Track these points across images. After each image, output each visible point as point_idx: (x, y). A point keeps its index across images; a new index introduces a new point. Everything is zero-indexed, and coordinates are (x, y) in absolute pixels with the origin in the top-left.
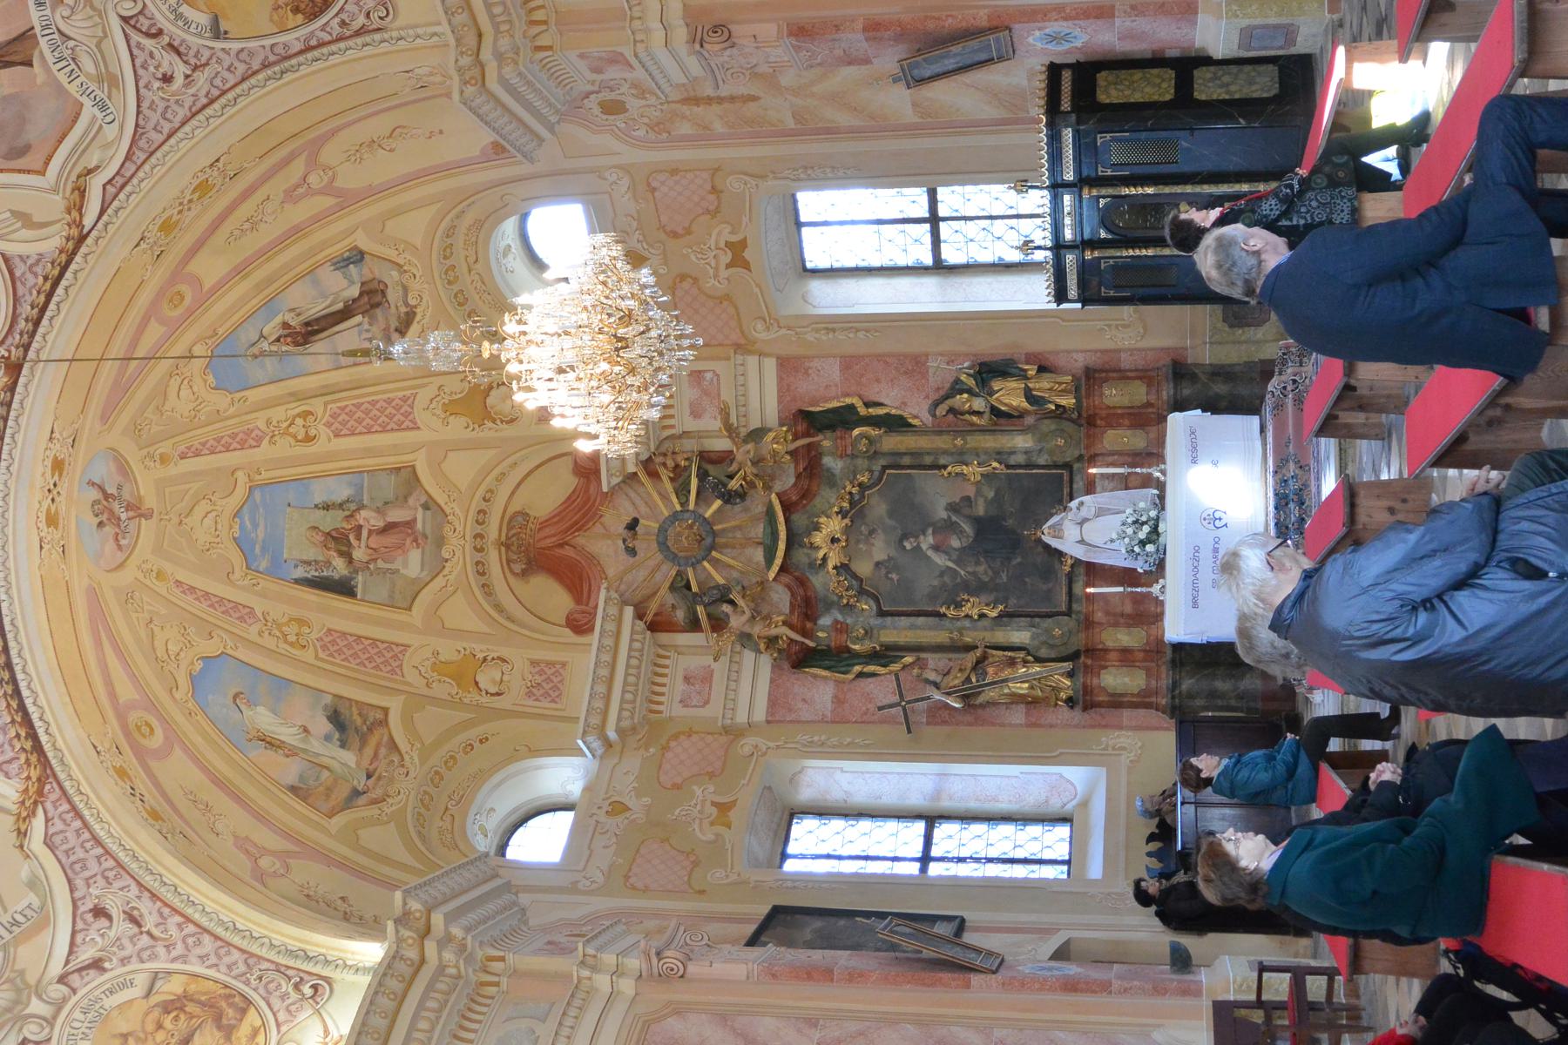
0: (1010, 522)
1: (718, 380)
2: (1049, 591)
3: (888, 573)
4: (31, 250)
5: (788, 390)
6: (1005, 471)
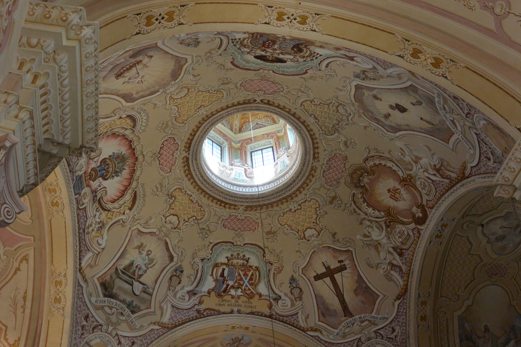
4: (300, 319)
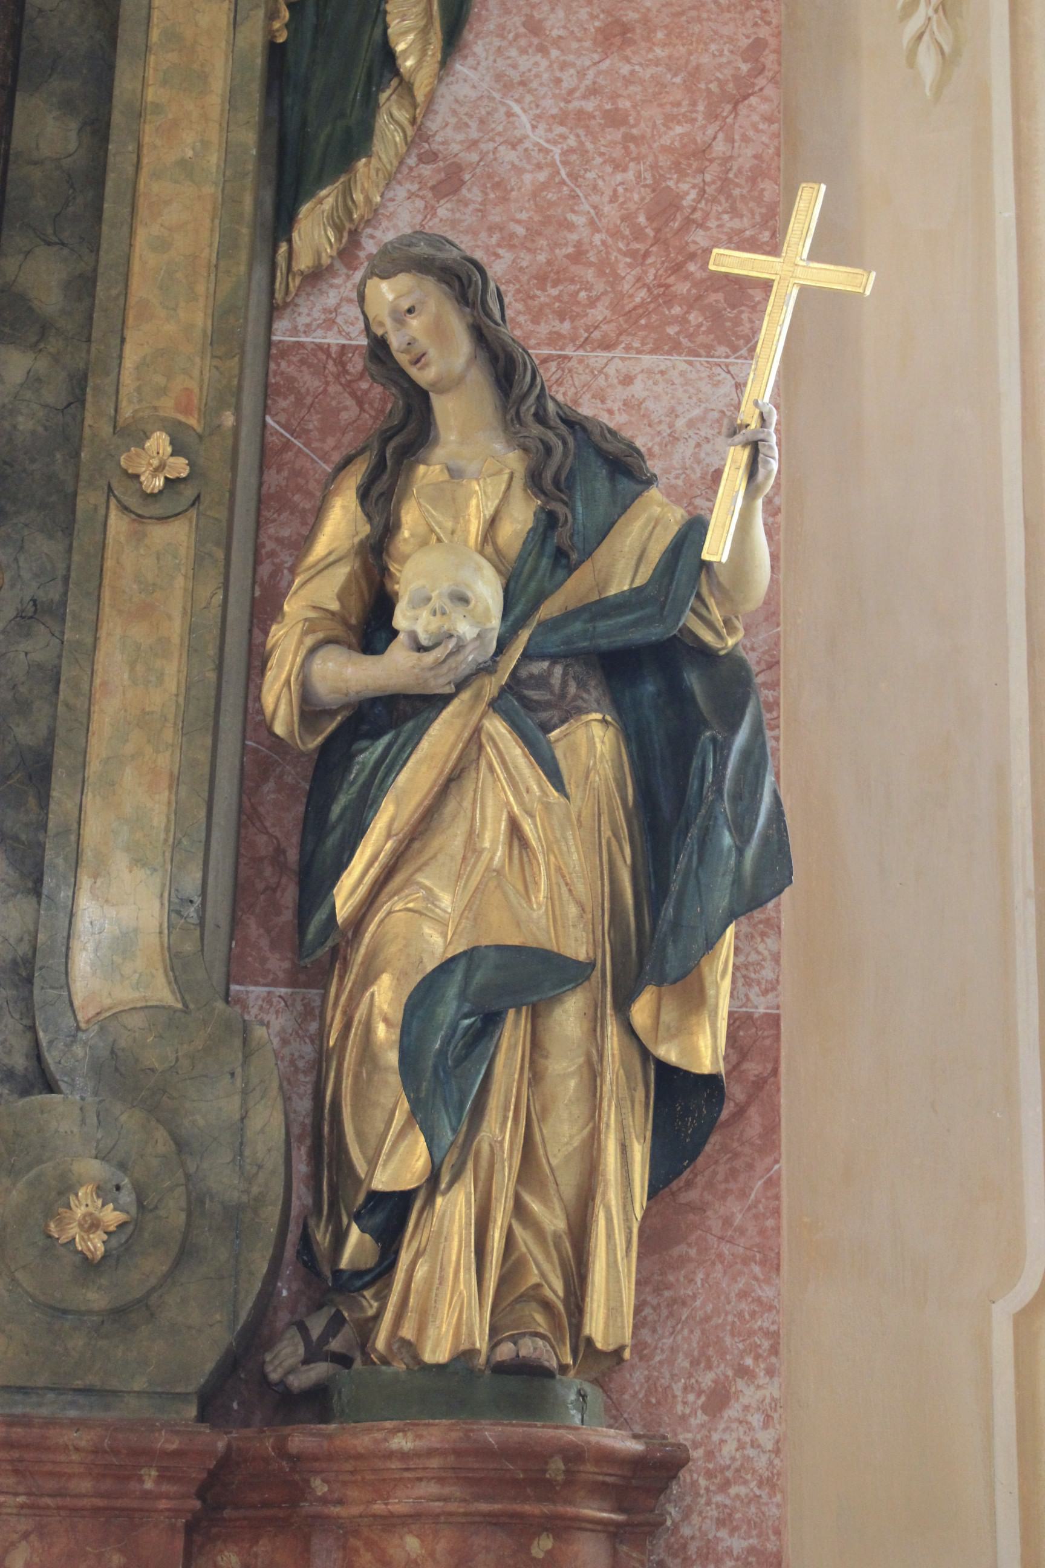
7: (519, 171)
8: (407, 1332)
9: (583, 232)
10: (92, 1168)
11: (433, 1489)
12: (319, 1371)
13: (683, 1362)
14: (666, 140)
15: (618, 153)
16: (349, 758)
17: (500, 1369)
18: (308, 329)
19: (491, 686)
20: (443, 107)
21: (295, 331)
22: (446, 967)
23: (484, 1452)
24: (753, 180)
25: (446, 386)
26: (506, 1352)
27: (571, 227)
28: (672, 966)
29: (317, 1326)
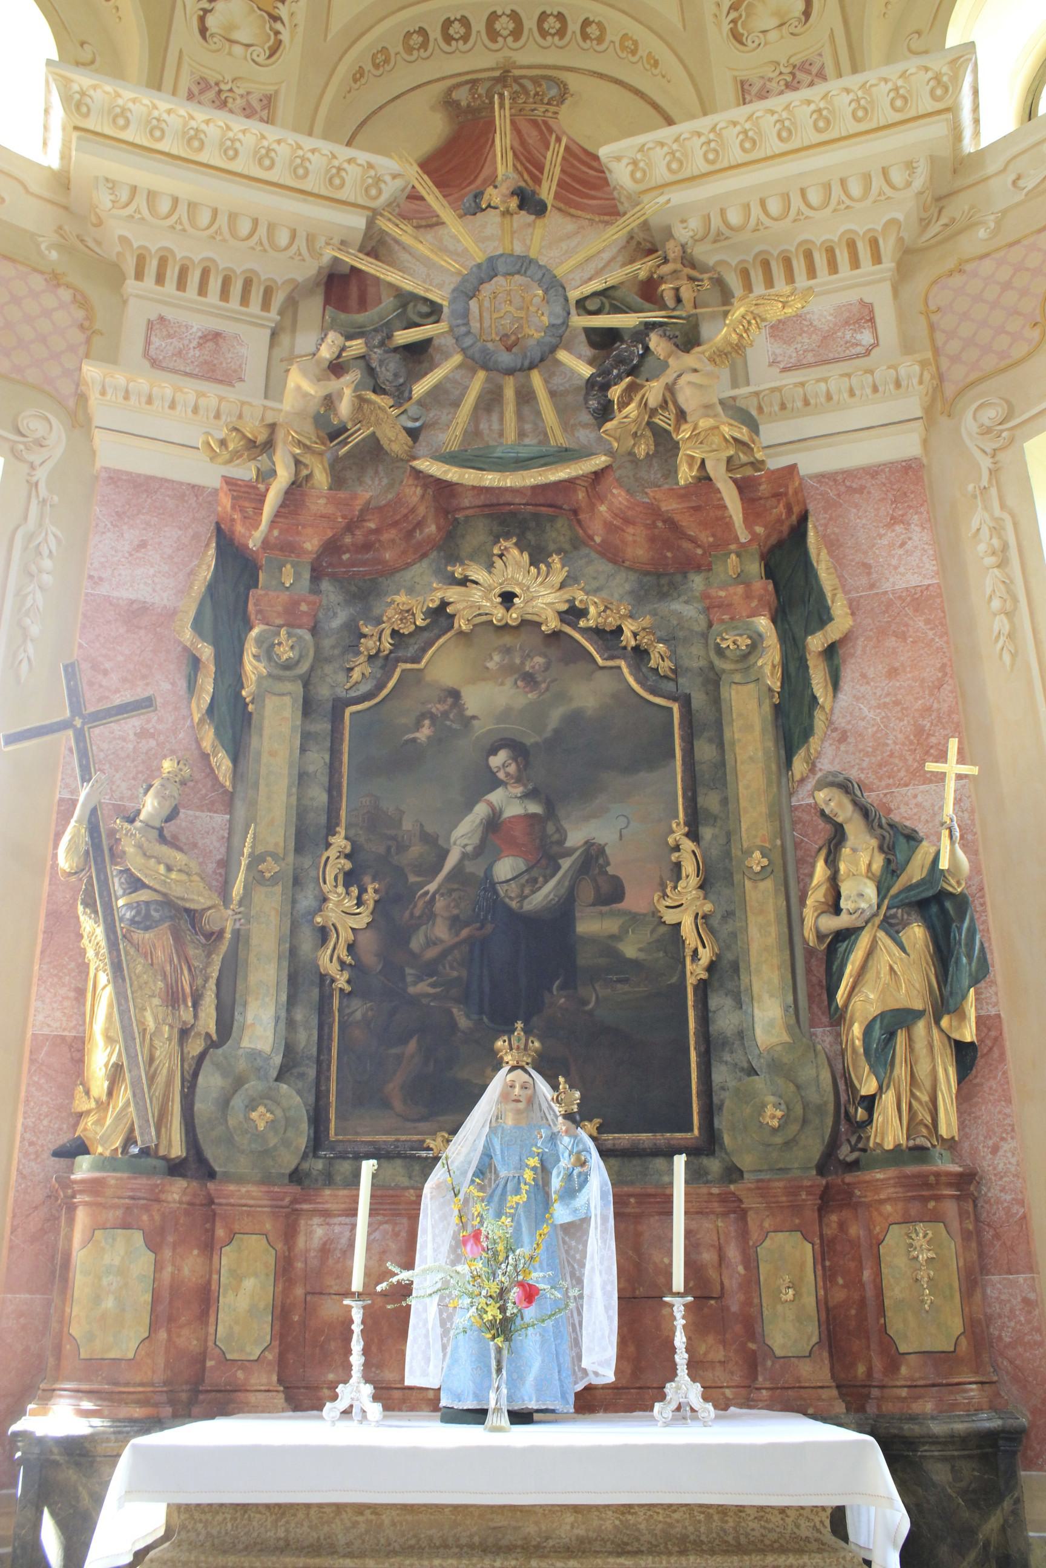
0: (558, 999)
1: (858, 356)
2: (385, 1104)
3: (433, 717)
5: (851, 490)
6: (691, 981)
7: (866, 728)
8: (878, 1140)
9: (892, 746)
10: (771, 1099)
11: (891, 1190)
12: (855, 1155)
13: (981, 1138)
14: (916, 707)
15: (900, 715)
16: (836, 950)
17: (911, 1149)
18: (803, 799)
19: (877, 921)
20: (836, 711)
21: (798, 801)
22: (874, 1019)
23: (906, 1177)
24: (949, 715)
25: (850, 820)
26: (911, 1143)
27: (887, 745)
28: (952, 1007)
29: (853, 1140)
